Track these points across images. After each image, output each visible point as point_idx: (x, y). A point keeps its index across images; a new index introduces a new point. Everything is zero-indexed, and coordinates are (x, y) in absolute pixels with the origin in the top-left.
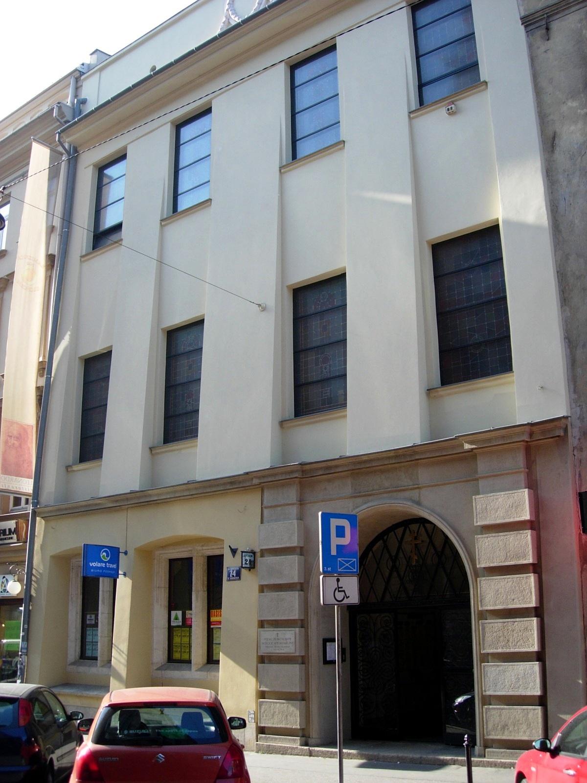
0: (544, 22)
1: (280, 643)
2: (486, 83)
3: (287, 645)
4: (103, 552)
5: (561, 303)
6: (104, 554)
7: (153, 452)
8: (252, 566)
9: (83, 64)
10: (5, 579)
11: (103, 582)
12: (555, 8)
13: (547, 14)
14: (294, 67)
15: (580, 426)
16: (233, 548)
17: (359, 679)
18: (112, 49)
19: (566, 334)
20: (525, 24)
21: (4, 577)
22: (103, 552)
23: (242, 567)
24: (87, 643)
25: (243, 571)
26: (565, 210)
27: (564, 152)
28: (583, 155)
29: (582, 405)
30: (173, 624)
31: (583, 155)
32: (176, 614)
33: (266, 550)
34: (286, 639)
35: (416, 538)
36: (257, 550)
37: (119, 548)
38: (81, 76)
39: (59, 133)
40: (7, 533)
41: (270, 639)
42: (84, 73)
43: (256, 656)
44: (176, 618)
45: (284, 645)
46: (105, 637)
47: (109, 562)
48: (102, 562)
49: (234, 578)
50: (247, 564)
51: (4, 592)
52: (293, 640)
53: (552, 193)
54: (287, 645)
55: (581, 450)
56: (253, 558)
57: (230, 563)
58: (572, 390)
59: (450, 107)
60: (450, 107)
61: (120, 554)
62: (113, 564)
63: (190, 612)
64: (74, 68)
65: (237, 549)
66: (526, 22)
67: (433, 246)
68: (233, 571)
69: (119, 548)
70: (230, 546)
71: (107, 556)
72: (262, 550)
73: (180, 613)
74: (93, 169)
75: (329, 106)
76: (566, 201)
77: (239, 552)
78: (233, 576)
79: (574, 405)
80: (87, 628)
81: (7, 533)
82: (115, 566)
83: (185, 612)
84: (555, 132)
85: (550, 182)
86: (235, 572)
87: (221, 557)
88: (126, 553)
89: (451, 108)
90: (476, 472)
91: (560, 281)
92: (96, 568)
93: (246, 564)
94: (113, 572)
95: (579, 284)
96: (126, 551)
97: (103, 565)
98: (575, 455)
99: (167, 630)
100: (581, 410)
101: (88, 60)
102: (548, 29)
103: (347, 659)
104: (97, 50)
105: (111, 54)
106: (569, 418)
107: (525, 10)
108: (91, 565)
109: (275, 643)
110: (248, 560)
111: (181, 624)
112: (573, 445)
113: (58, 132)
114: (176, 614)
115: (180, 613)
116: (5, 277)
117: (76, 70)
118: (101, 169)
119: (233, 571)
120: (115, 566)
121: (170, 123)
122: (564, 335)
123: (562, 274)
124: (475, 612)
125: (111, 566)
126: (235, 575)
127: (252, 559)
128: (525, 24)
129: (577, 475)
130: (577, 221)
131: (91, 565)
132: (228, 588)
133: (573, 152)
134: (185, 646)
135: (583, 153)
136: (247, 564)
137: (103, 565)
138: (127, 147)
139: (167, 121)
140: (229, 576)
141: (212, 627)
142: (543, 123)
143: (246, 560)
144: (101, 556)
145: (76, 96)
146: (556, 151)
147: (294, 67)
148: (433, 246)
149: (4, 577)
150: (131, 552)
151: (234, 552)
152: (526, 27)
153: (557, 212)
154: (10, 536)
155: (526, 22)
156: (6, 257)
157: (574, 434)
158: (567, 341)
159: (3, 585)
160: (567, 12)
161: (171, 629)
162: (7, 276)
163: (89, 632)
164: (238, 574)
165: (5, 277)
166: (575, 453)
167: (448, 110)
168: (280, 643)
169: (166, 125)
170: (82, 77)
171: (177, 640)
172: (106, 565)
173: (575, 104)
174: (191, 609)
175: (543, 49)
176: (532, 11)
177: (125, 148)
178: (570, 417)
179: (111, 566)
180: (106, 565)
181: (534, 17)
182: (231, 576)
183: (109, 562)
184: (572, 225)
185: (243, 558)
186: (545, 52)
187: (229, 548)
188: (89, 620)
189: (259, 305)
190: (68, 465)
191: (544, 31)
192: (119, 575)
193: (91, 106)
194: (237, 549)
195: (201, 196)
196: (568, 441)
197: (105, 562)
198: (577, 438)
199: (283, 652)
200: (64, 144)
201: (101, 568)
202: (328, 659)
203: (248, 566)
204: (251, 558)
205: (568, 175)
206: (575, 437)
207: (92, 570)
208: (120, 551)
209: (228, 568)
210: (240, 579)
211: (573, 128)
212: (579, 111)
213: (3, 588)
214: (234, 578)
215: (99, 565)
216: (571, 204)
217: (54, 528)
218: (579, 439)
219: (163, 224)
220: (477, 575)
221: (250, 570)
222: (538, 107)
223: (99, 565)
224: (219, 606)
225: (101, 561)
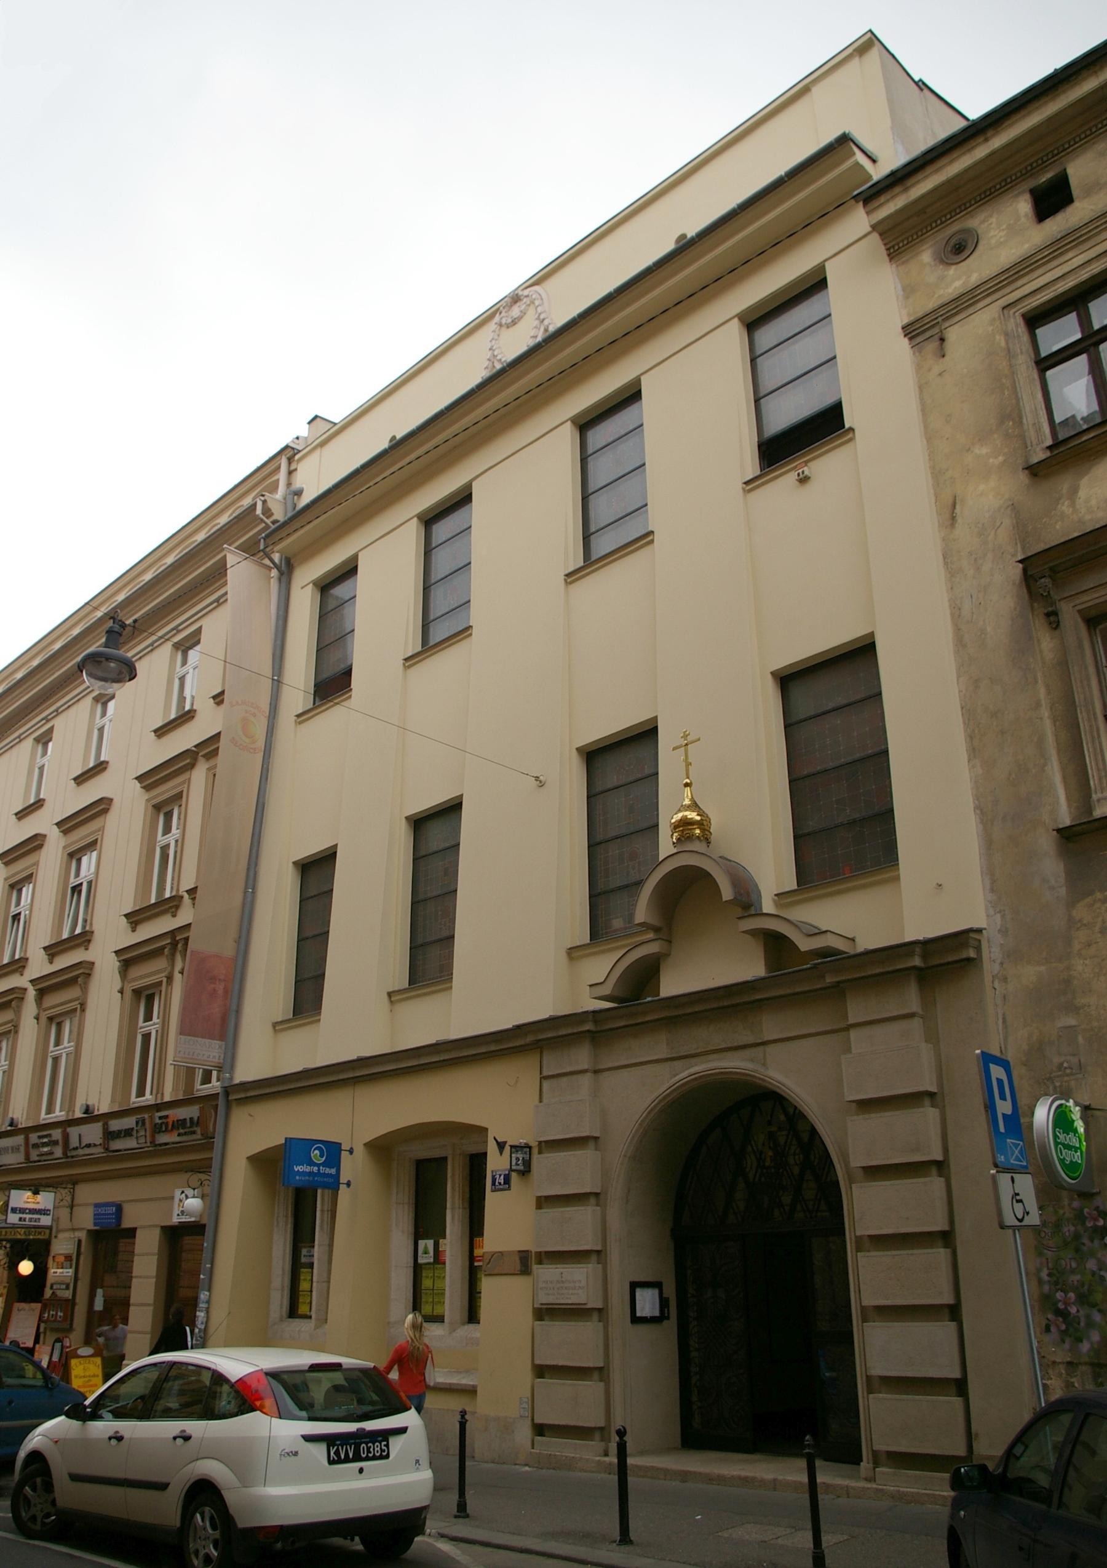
0: (936, 330)
1: (566, 1288)
2: (851, 429)
3: (576, 1291)
4: (314, 1150)
5: (969, 756)
6: (317, 1152)
7: (392, 999)
8: (526, 1171)
9: (298, 438)
10: (183, 1195)
11: (323, 1196)
12: (953, 306)
13: (941, 316)
14: (585, 424)
15: (1002, 942)
16: (499, 1140)
17: (692, 1349)
18: (337, 414)
19: (977, 802)
20: (910, 336)
21: (183, 1192)
22: (314, 1150)
23: (511, 1170)
24: (301, 1293)
25: (514, 1175)
26: (973, 613)
27: (968, 525)
28: (998, 528)
29: (1004, 911)
30: (420, 1261)
31: (998, 528)
32: (426, 1244)
33: (546, 1142)
34: (574, 1282)
35: (769, 1123)
36: (534, 1144)
37: (340, 1144)
38: (295, 454)
39: (265, 540)
40: (188, 1125)
41: (551, 1282)
42: (299, 451)
43: (530, 1309)
44: (426, 1252)
45: (571, 1292)
46: (324, 1282)
47: (324, 1164)
48: (315, 1164)
49: (501, 1187)
50: (518, 1165)
51: (183, 1215)
52: (584, 1283)
53: (952, 588)
54: (576, 1291)
55: (1005, 980)
56: (528, 1156)
57: (496, 1163)
58: (988, 887)
59: (800, 471)
60: (800, 471)
61: (343, 1152)
62: (331, 1167)
63: (445, 1241)
64: (283, 445)
65: (505, 1143)
66: (910, 333)
67: (781, 678)
68: (500, 1175)
69: (340, 1144)
70: (495, 1139)
71: (322, 1156)
72: (540, 1143)
73: (430, 1243)
74: (313, 589)
75: (823, 374)
76: (974, 600)
77: (507, 1149)
78: (500, 1184)
79: (991, 912)
80: (302, 1270)
81: (188, 1125)
82: (333, 1171)
83: (438, 1241)
84: (955, 497)
85: (950, 573)
86: (502, 1177)
87: (484, 1155)
88: (351, 1151)
89: (803, 472)
90: (845, 1016)
91: (967, 722)
92: (303, 1173)
93: (517, 1164)
94: (331, 1180)
95: (995, 724)
96: (352, 1148)
97: (315, 1169)
98: (995, 989)
99: (412, 1270)
100: (1003, 917)
101: (304, 431)
102: (942, 340)
103: (671, 1315)
104: (316, 417)
105: (336, 421)
106: (984, 931)
107: (909, 315)
108: (296, 1170)
109: (558, 1289)
110: (521, 1159)
111: (432, 1260)
112: (991, 972)
113: (263, 538)
114: (426, 1244)
115: (430, 1243)
116: (194, 749)
117: (287, 447)
118: (326, 586)
119: (500, 1175)
120: (333, 1171)
121: (311, 585)
122: (974, 803)
123: (969, 710)
124: (851, 1239)
125: (328, 1171)
126: (502, 1182)
127: (527, 1157)
128: (910, 336)
129: (1000, 1021)
130: (989, 629)
131: (296, 1170)
132: (493, 1201)
133: (983, 524)
134: (426, 1294)
135: (998, 524)
136: (518, 1165)
137: (315, 1169)
138: (357, 555)
139: (411, 516)
140: (494, 1183)
141: (476, 1264)
142: (938, 484)
143: (518, 1159)
144: (312, 1155)
145: (289, 484)
146: (957, 525)
147: (585, 424)
148: (781, 678)
149: (183, 1192)
150: (359, 1150)
151: (501, 1146)
152: (911, 339)
153: (959, 616)
154: (192, 1129)
155: (910, 333)
156: (194, 720)
157: (992, 954)
158: (978, 812)
159: (181, 1205)
160: (971, 310)
161: (417, 1269)
162: (195, 746)
163: (304, 1273)
164: (507, 1180)
165: (194, 749)
166: (996, 985)
167: (799, 475)
168: (566, 1288)
169: (411, 521)
170: (297, 457)
171: (427, 1283)
172: (319, 1170)
173: (984, 451)
174: (445, 1238)
175: (936, 369)
176: (920, 314)
177: (354, 559)
178: (985, 929)
179: (328, 1171)
180: (319, 1170)
181: (975, 294)
182: (497, 1184)
183: (324, 1164)
184: (983, 636)
185: (513, 1155)
186: (940, 374)
187: (495, 1142)
188: (304, 1256)
189: (537, 778)
190: (275, 1021)
191: (938, 343)
192: (341, 1185)
193: (305, 500)
194: (505, 1143)
195: (631, 530)
196: (982, 967)
197: (318, 1165)
198: (998, 961)
199: (570, 1302)
200: (272, 556)
201: (311, 1174)
202: (638, 1314)
203: (521, 1168)
204: (525, 1156)
205: (976, 560)
206: (994, 961)
207: (297, 1178)
208: (343, 1148)
209: (492, 1172)
210: (509, 1189)
211: (982, 487)
212: (991, 460)
213: (181, 1209)
214: (501, 1187)
215: (308, 1169)
216: (980, 603)
217: (251, 1116)
218: (1002, 964)
219: (569, 580)
220: (851, 1181)
221: (523, 1175)
222: (930, 459)
223: (308, 1169)
224: (481, 1234)
225: (311, 1163)
